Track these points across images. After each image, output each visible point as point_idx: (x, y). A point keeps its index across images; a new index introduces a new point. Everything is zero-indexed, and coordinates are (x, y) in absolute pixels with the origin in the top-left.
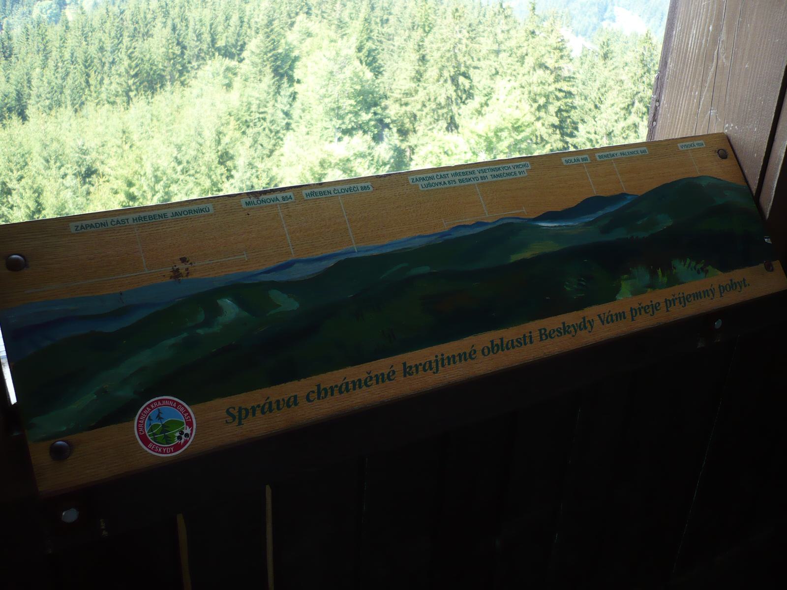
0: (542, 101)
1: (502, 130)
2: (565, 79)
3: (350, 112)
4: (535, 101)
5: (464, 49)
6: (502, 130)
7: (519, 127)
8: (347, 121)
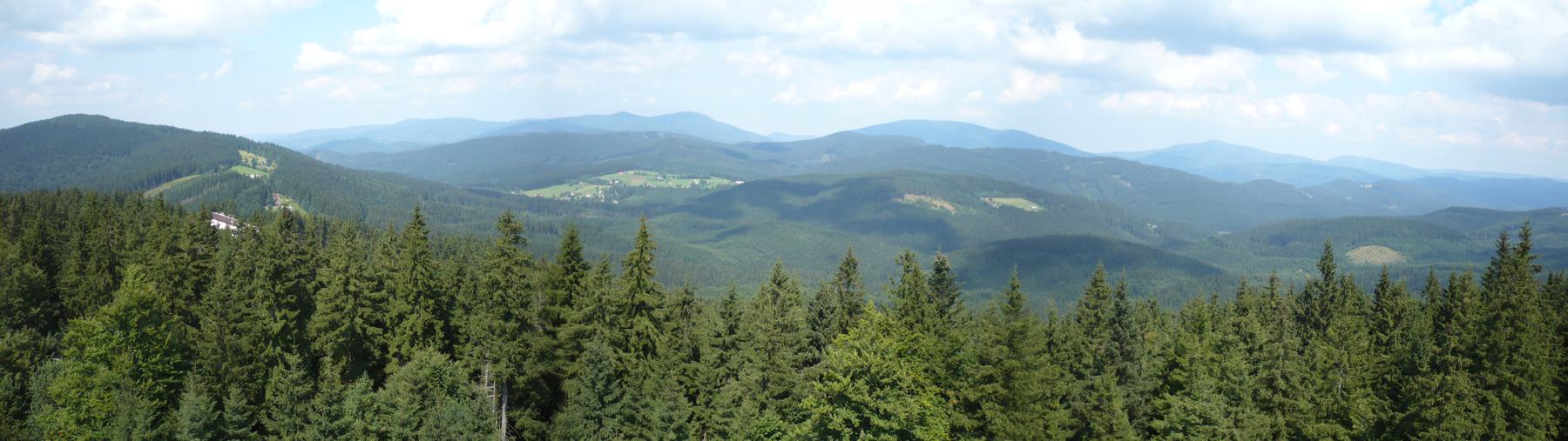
0: (177, 278)
1: (131, 309)
2: (201, 257)
3: (19, 309)
4: (171, 279)
5: (116, 242)
6: (131, 309)
7: (145, 303)
8: (17, 317)
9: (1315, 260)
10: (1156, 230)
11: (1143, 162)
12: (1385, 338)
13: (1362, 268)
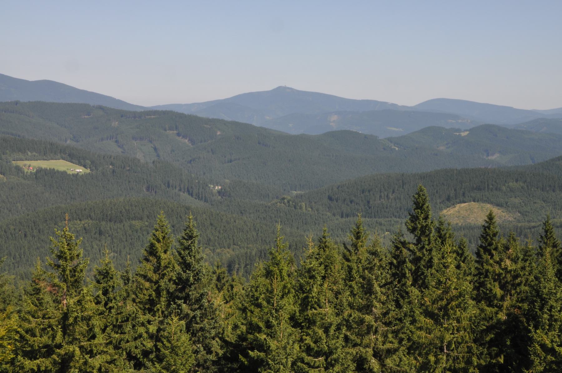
9: (404, 221)
10: (219, 192)
11: (200, 115)
12: (197, 339)
13: (461, 228)
